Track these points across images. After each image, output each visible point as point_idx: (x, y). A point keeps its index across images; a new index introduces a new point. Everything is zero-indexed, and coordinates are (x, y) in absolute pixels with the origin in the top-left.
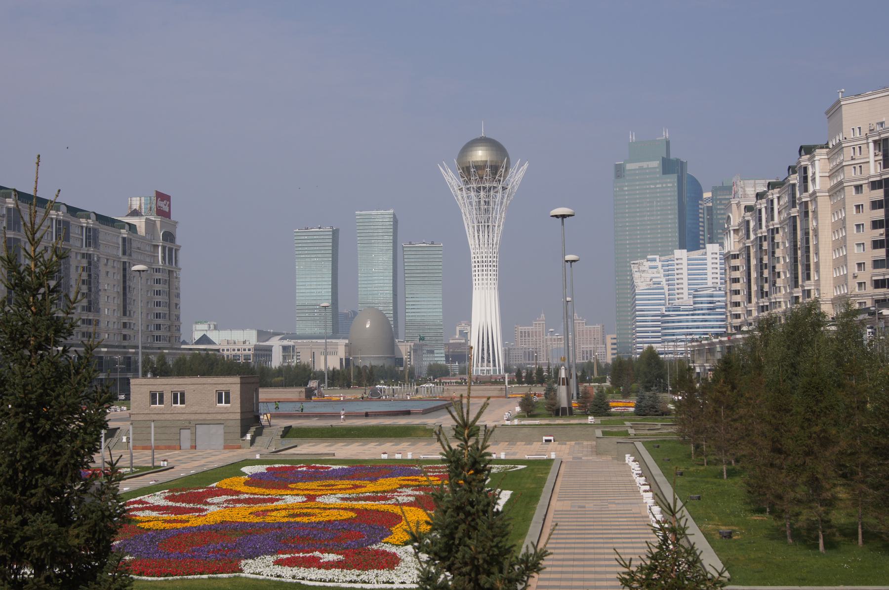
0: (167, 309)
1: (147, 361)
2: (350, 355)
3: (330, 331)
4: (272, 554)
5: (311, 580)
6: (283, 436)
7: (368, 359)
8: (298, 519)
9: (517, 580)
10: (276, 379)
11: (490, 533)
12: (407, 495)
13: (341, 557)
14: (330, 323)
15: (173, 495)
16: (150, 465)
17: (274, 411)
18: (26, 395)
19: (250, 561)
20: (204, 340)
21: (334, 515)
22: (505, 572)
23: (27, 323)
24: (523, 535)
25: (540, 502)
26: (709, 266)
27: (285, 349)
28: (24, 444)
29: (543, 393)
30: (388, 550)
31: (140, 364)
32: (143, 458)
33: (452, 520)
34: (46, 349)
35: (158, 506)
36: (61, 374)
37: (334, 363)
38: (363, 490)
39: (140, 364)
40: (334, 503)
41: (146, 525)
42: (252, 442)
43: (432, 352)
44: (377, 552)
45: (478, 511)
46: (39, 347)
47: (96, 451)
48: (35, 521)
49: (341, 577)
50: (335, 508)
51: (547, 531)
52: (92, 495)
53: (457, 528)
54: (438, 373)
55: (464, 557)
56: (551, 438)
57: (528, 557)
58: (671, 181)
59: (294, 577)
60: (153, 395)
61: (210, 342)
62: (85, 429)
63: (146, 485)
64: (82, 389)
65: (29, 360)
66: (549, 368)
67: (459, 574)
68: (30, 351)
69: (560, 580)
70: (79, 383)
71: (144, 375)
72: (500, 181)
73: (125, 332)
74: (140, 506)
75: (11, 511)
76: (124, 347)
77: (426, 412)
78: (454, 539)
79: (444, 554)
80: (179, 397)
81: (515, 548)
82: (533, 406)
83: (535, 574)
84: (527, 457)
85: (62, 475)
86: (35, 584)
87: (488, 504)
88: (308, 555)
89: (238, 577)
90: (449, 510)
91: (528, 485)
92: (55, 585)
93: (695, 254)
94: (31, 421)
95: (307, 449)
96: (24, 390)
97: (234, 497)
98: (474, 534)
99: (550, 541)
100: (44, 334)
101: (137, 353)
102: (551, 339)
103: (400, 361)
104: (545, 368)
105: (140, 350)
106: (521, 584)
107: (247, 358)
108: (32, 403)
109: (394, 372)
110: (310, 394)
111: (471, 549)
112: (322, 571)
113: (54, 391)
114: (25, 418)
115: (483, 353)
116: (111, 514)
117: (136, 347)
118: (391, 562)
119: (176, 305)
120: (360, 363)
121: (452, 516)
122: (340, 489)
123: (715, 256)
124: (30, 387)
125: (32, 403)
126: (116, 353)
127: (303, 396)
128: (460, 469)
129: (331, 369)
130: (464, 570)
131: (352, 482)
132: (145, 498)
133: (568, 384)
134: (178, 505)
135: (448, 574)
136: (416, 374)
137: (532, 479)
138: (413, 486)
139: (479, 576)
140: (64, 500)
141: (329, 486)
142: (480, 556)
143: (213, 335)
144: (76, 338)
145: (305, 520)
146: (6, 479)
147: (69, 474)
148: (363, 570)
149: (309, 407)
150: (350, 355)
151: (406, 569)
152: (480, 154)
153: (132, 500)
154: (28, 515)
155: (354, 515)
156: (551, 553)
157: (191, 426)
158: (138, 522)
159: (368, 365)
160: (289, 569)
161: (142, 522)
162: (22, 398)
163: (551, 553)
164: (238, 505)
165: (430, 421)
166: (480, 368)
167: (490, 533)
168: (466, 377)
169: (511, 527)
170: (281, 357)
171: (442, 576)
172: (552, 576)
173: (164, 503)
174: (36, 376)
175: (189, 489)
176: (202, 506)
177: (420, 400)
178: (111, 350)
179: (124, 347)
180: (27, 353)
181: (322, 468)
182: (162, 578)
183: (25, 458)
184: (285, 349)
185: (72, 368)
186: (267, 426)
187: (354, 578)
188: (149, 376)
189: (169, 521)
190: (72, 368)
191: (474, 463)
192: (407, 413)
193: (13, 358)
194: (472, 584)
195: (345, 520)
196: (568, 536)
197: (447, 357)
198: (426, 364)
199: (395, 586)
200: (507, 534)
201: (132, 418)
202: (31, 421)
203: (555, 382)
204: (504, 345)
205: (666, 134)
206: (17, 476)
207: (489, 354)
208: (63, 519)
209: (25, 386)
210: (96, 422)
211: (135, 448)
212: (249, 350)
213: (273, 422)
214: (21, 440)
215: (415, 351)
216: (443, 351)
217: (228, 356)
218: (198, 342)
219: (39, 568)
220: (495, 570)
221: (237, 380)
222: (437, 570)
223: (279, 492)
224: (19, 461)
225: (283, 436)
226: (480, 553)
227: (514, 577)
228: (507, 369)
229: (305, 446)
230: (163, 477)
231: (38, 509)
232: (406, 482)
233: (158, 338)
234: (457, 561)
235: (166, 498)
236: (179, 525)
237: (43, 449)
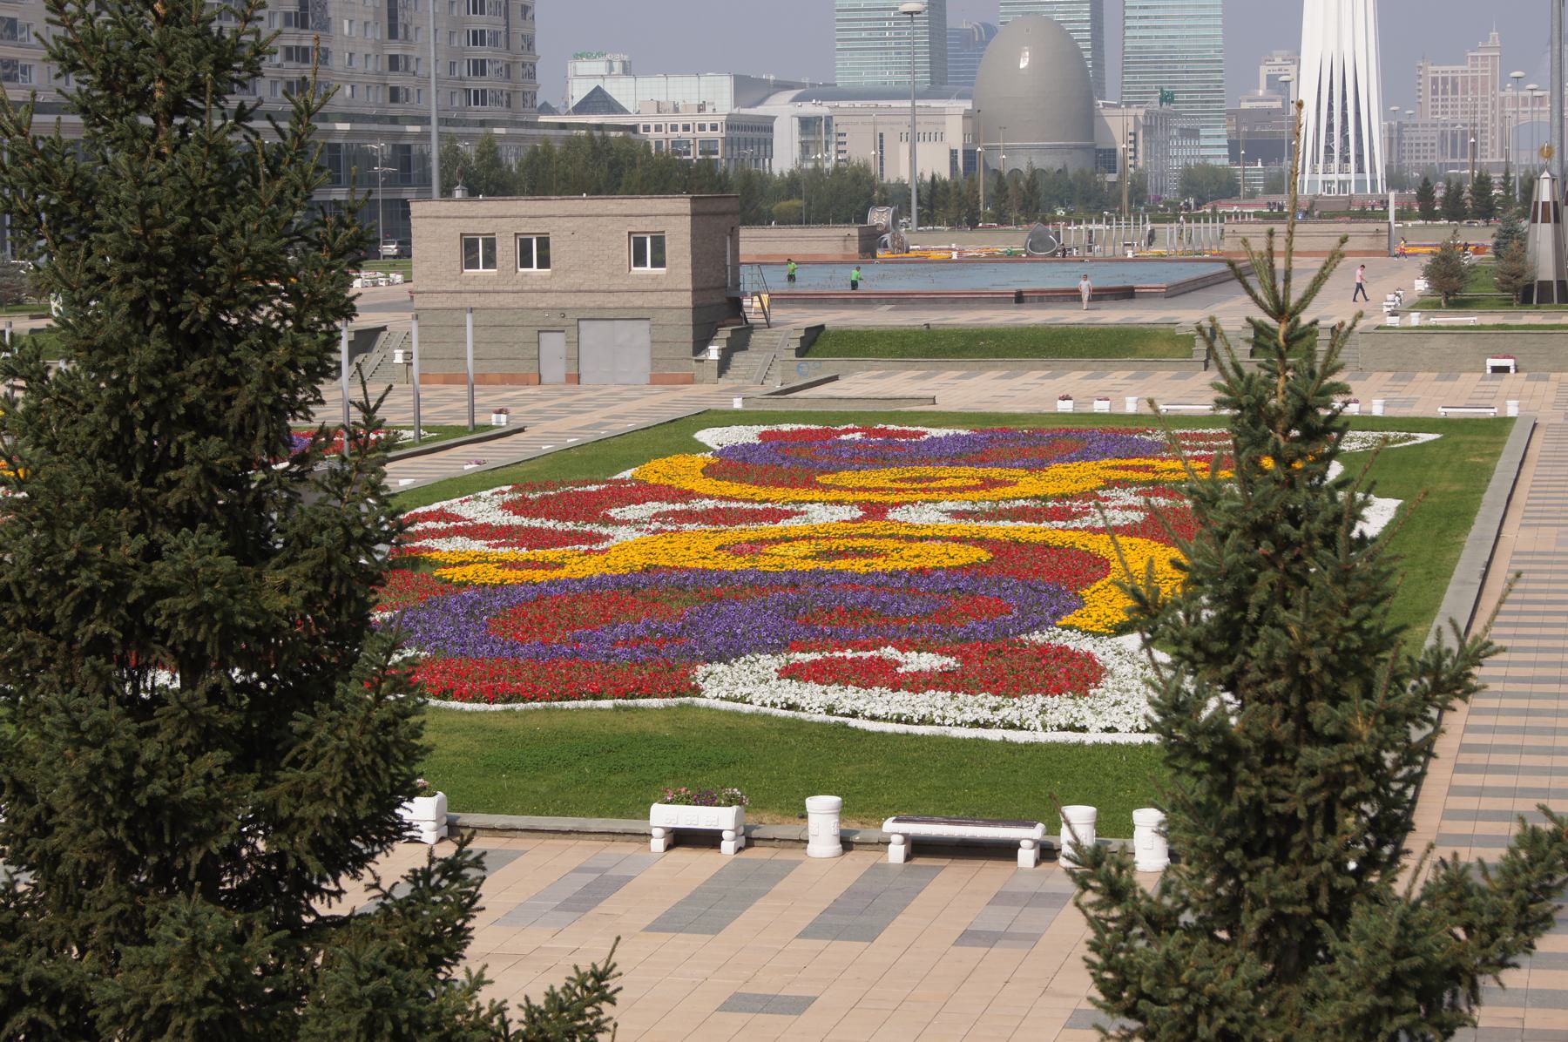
0: (501, 20)
1: (451, 158)
2: (976, 141)
3: (923, 79)
4: (775, 650)
5: (873, 718)
6: (801, 352)
7: (1025, 152)
8: (842, 564)
9: (1410, 718)
10: (785, 204)
11: (1340, 594)
12: (1124, 507)
13: (951, 662)
14: (923, 58)
15: (526, 499)
16: (465, 423)
17: (782, 286)
18: (147, 230)
19: (719, 668)
20: (598, 100)
21: (934, 556)
22: (1379, 694)
23: (144, 44)
24: (1426, 613)
25: (1475, 530)
27: (807, 124)
28: (146, 353)
29: (1490, 242)
30: (1072, 645)
31: (435, 165)
32: (446, 405)
33: (1241, 558)
34: (197, 113)
35: (487, 526)
36: (231, 178)
37: (934, 163)
38: (1009, 491)
39: (435, 165)
40: (933, 523)
41: (457, 574)
42: (723, 366)
43: (1193, 134)
44: (1043, 650)
45: (1309, 536)
46: (177, 106)
47: (326, 373)
48: (178, 549)
49: (952, 713)
50: (934, 538)
51: (1489, 603)
52: (320, 485)
53: (1253, 579)
54: (1207, 191)
55: (1270, 654)
56: (1510, 362)
57: (1439, 659)
59: (830, 710)
60: (469, 245)
61: (611, 106)
62: (298, 319)
63: (453, 471)
64: (288, 214)
65: (153, 139)
66: (1507, 177)
67: (1258, 699)
68: (155, 117)
69: (1523, 730)
70: (279, 201)
71: (447, 192)
73: (395, 80)
74: (442, 525)
75: (119, 524)
76: (394, 120)
77: (1176, 292)
78: (1244, 607)
79: (1217, 647)
80: (534, 251)
81: (1405, 635)
82: (1463, 277)
83: (1457, 703)
84: (1441, 412)
85: (243, 435)
86: (183, 705)
87: (1337, 519)
88: (866, 655)
89: (690, 706)
90: (1234, 533)
91: (1443, 486)
92: (232, 708)
94: (161, 296)
95: (863, 385)
96: (144, 217)
97: (678, 507)
98: (1298, 597)
99: (1499, 619)
100: (187, 74)
101: (425, 136)
102: (1515, 99)
103: (1107, 159)
104: (1496, 177)
105: (434, 128)
106: (1419, 726)
107: (708, 148)
108: (162, 250)
109: (1087, 188)
110: (871, 242)
111: (1288, 634)
112: (903, 695)
113: (217, 221)
114: (148, 290)
115: (1330, 137)
116: (367, 534)
117: (424, 120)
118: (1079, 676)
119: (525, 9)
120: (1004, 162)
121: (1241, 549)
122: (950, 490)
124: (156, 210)
125: (162, 250)
126: (374, 136)
127: (854, 248)
128: (1263, 427)
129: (928, 178)
130: (1270, 687)
131: (981, 472)
132: (454, 505)
133: (1557, 220)
134: (536, 523)
135: (1228, 696)
136: (1151, 193)
137: (1454, 470)
138: (1138, 483)
139: (1310, 705)
140: (249, 498)
141: (920, 480)
142: (1313, 653)
143: (619, 90)
144: (268, 92)
145: (859, 566)
146: (104, 443)
147: (262, 432)
148: (1007, 695)
149: (873, 278)
150: (976, 141)
151: (1118, 696)
153: (420, 510)
154: (162, 534)
155: (983, 555)
156: (1503, 649)
157: (567, 322)
158: (435, 564)
159: (1024, 168)
160: (819, 688)
161: (445, 565)
162: (138, 238)
163: (1503, 649)
164: (687, 527)
165: (1187, 316)
166: (1321, 177)
167: (1340, 594)
168: (1283, 199)
169: (1395, 581)
170: (797, 148)
171: (1213, 703)
172: (1507, 703)
173: (499, 518)
174: (170, 182)
175: (563, 484)
176: (596, 528)
177: (1161, 259)
178: (359, 127)
179: (394, 120)
180: (146, 121)
181: (903, 434)
182: (498, 707)
183: (150, 389)
184: (807, 124)
185: (261, 161)
186: (760, 327)
187: (985, 714)
188: (458, 194)
189: (515, 565)
190: (261, 161)
191: (1302, 413)
192: (1126, 294)
193: (113, 135)
194: (1291, 724)
195: (962, 567)
196: (1547, 619)
197: (1233, 147)
198: (1176, 164)
199: (1088, 739)
200: (1384, 597)
201: (417, 303)
202: (161, 296)
203: (1525, 215)
204: (1386, 114)
206: (133, 435)
207: (1345, 138)
208: (251, 549)
209: (144, 207)
210: (324, 301)
211: (424, 378)
212: (714, 128)
213: (777, 314)
214: (139, 345)
215: (1149, 130)
216: (1222, 131)
217: (659, 144)
218: (581, 108)
219: (191, 667)
220: (1353, 688)
221: (683, 204)
222: (1200, 685)
223: (792, 494)
224: (136, 397)
225: (801, 352)
226: (1312, 644)
227: (1401, 707)
228: (1394, 181)
229: (860, 376)
230: (497, 453)
231: (187, 518)
232: (1122, 474)
233: (479, 97)
234: (1251, 664)
235: (506, 506)
236: (539, 576)
237: (195, 367)
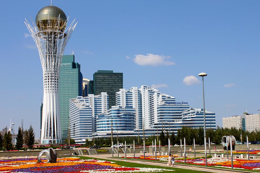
58: (77, 69)
93: (97, 96)
123: (105, 97)
152: (46, 14)
205: (73, 53)
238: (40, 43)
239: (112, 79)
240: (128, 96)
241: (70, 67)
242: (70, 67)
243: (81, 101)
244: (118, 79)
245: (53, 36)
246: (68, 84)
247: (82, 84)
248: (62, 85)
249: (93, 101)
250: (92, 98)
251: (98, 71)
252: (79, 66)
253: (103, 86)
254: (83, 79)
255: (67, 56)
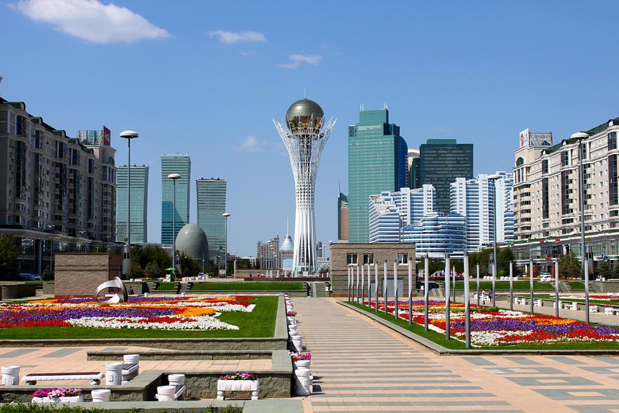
26: (425, 200)
58: (391, 138)
72: (318, 131)
93: (415, 191)
152: (299, 110)
205: (386, 107)
238: (290, 144)
239: (451, 155)
240: (471, 193)
241: (380, 134)
242: (380, 134)
243: (386, 200)
244: (463, 155)
245: (305, 140)
246: (376, 164)
247: (407, 160)
248: (366, 166)
249: (408, 200)
250: (406, 194)
251: (429, 140)
252: (397, 129)
253: (437, 169)
254: (409, 151)
255: (372, 113)
